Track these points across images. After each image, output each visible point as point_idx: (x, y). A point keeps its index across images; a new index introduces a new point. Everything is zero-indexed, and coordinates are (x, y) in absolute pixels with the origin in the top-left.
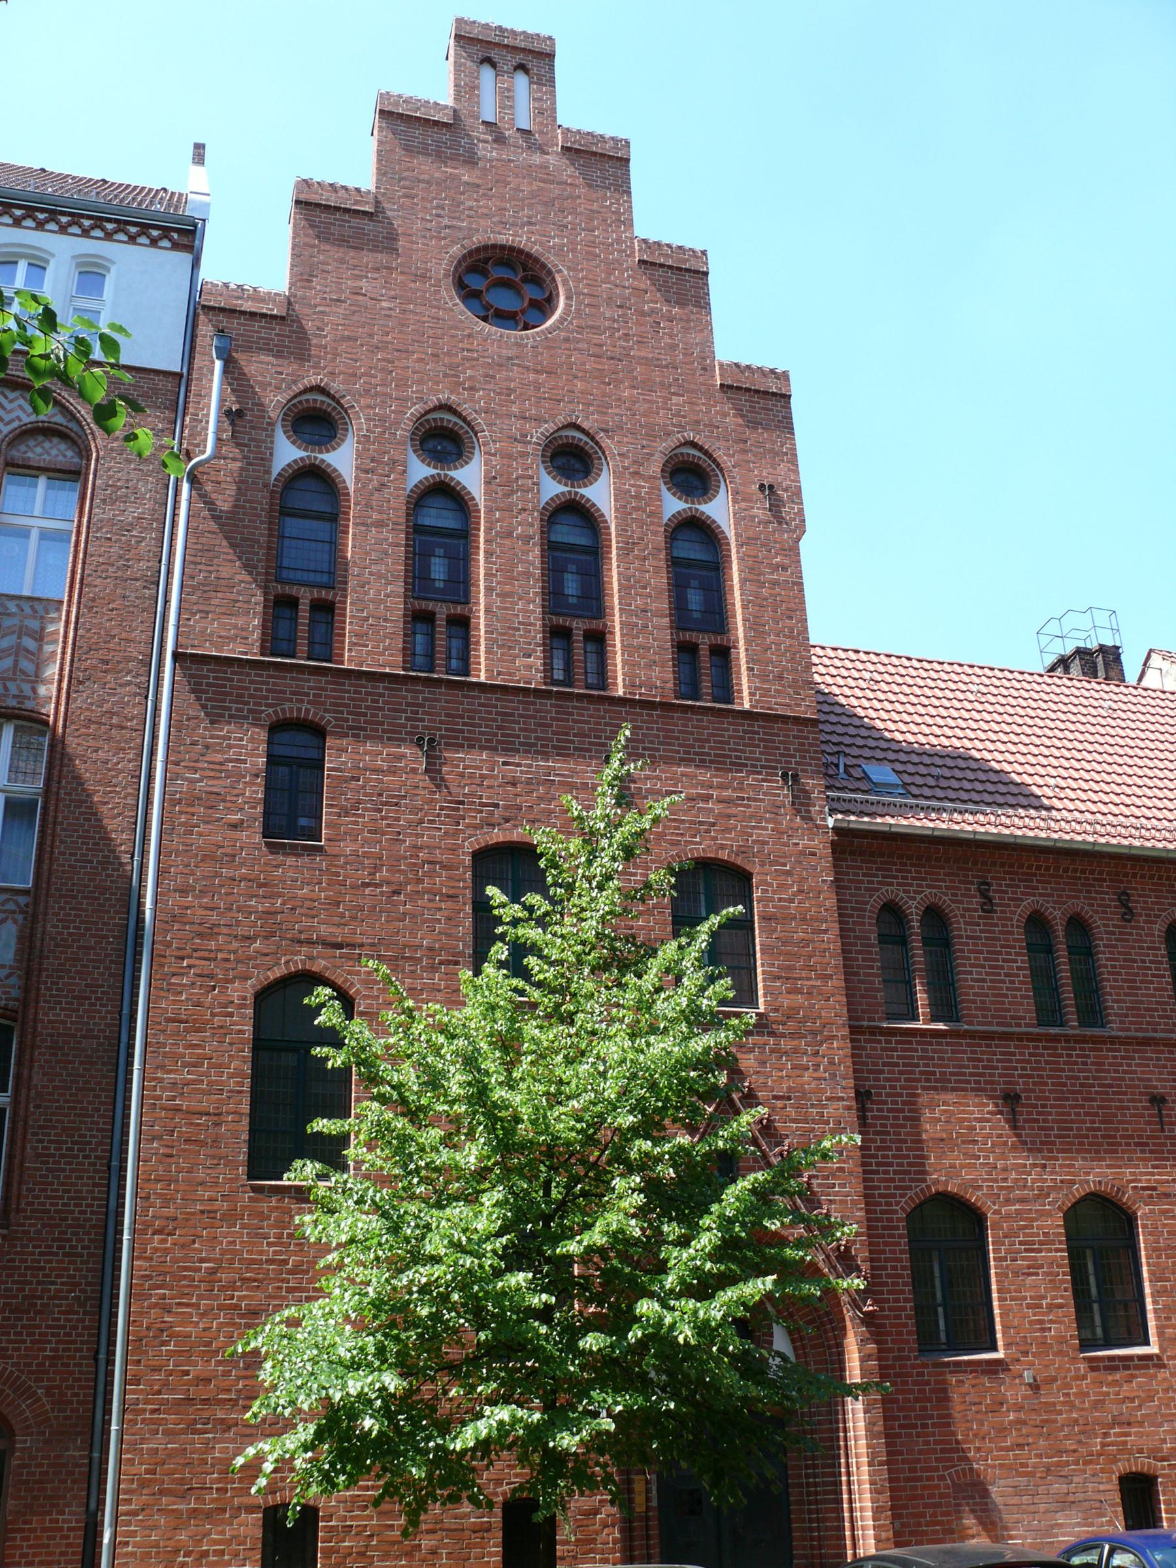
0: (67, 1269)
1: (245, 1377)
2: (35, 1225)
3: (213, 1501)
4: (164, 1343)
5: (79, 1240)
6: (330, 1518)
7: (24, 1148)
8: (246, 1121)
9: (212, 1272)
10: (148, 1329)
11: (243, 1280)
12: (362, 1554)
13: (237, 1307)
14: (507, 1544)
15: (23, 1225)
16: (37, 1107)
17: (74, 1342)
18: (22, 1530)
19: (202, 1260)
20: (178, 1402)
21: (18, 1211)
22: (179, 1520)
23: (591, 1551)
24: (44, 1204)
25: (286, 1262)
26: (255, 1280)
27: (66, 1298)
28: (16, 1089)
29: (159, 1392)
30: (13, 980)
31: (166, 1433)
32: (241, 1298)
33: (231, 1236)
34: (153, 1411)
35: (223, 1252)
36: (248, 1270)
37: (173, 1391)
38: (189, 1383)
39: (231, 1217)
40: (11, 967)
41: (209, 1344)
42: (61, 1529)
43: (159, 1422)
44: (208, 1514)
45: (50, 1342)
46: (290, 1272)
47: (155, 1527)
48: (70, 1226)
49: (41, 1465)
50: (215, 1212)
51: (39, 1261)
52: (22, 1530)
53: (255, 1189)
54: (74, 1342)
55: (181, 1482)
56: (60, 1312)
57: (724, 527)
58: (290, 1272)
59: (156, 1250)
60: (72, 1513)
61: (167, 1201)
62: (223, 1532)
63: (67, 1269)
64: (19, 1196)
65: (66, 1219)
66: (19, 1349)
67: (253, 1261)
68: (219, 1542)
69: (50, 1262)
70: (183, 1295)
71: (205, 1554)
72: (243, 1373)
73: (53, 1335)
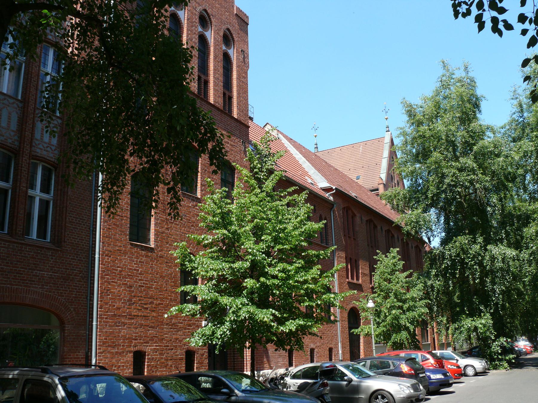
0: (79, 265)
1: (129, 308)
2: (69, 248)
3: (121, 349)
4: (109, 295)
5: (82, 255)
6: (148, 355)
7: (66, 218)
8: (129, 220)
9: (121, 271)
10: (104, 289)
11: (128, 275)
12: (156, 366)
13: (126, 284)
14: (186, 364)
15: (66, 247)
16: (70, 203)
17: (81, 292)
18: (68, 358)
19: (118, 267)
20: (112, 316)
21: (64, 242)
22: (113, 355)
23: (203, 366)
24: (72, 240)
25: (138, 270)
26: (131, 276)
27: (78, 276)
28: (15, 181)
29: (107, 312)
30: (56, 152)
31: (110, 326)
32: (128, 281)
33: (125, 259)
34: (106, 318)
35: (124, 265)
36: (130, 272)
37: (111, 312)
38: (115, 309)
39: (125, 253)
40: (56, 147)
41: (120, 296)
42: (79, 358)
43: (107, 322)
44: (120, 353)
45: (74, 292)
46: (140, 274)
47: (107, 358)
48: (79, 250)
49: (73, 336)
50: (121, 250)
51: (71, 261)
52: (68, 358)
53: (132, 244)
54: (81, 292)
55: (113, 342)
56: (77, 281)
57: (182, 19)
58: (140, 274)
59: (106, 262)
60: (82, 353)
61: (109, 245)
62: (123, 360)
63: (79, 265)
64: (65, 236)
65: (78, 247)
66: (65, 293)
67: (131, 269)
68: (122, 363)
69: (74, 262)
70: (113, 279)
71: (119, 366)
72: (128, 307)
73: (75, 289)
